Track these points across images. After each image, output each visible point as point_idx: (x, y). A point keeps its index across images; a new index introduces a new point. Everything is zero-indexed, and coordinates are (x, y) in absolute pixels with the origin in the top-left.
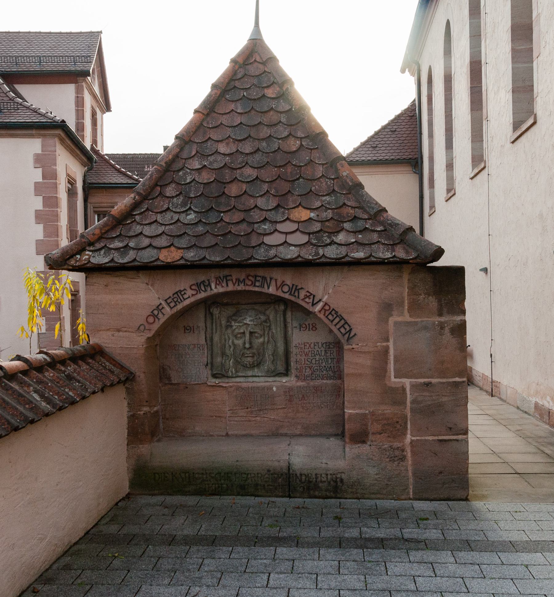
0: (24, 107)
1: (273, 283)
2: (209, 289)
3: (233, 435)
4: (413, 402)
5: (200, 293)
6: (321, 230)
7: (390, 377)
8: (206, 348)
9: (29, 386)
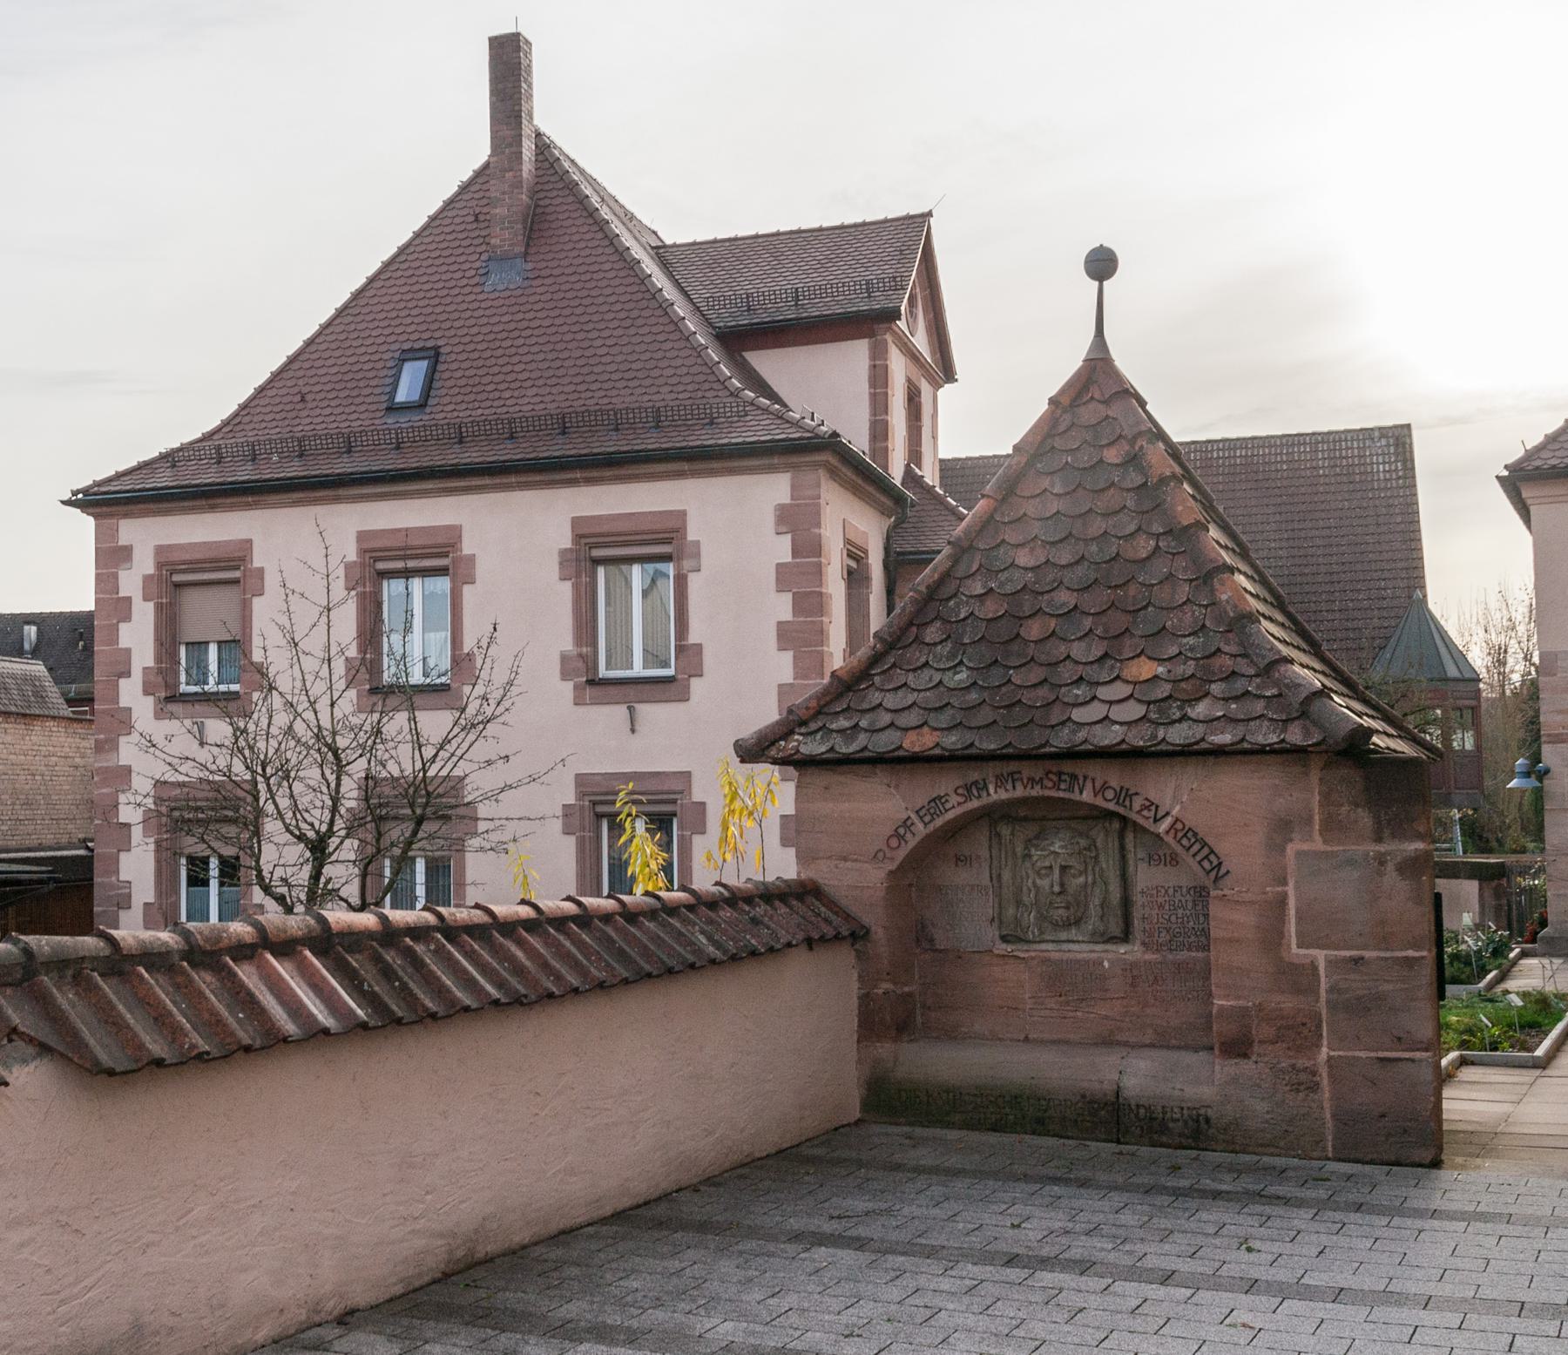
0: (759, 408)
1: (1089, 785)
3: (1035, 1040)
4: (1330, 990)
6: (1170, 697)
7: (1289, 946)
9: (695, 924)
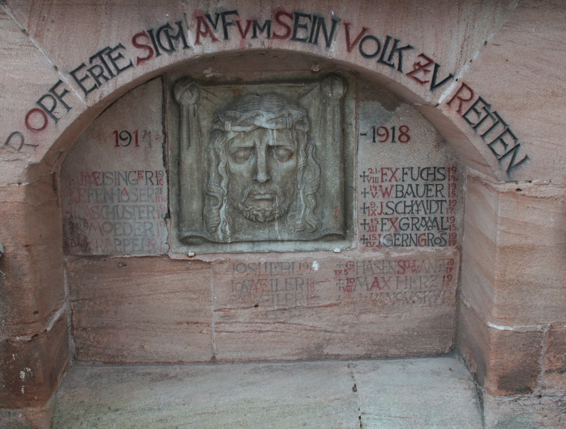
1: (340, 31)
2: (181, 45)
5: (158, 54)
8: (165, 180)
